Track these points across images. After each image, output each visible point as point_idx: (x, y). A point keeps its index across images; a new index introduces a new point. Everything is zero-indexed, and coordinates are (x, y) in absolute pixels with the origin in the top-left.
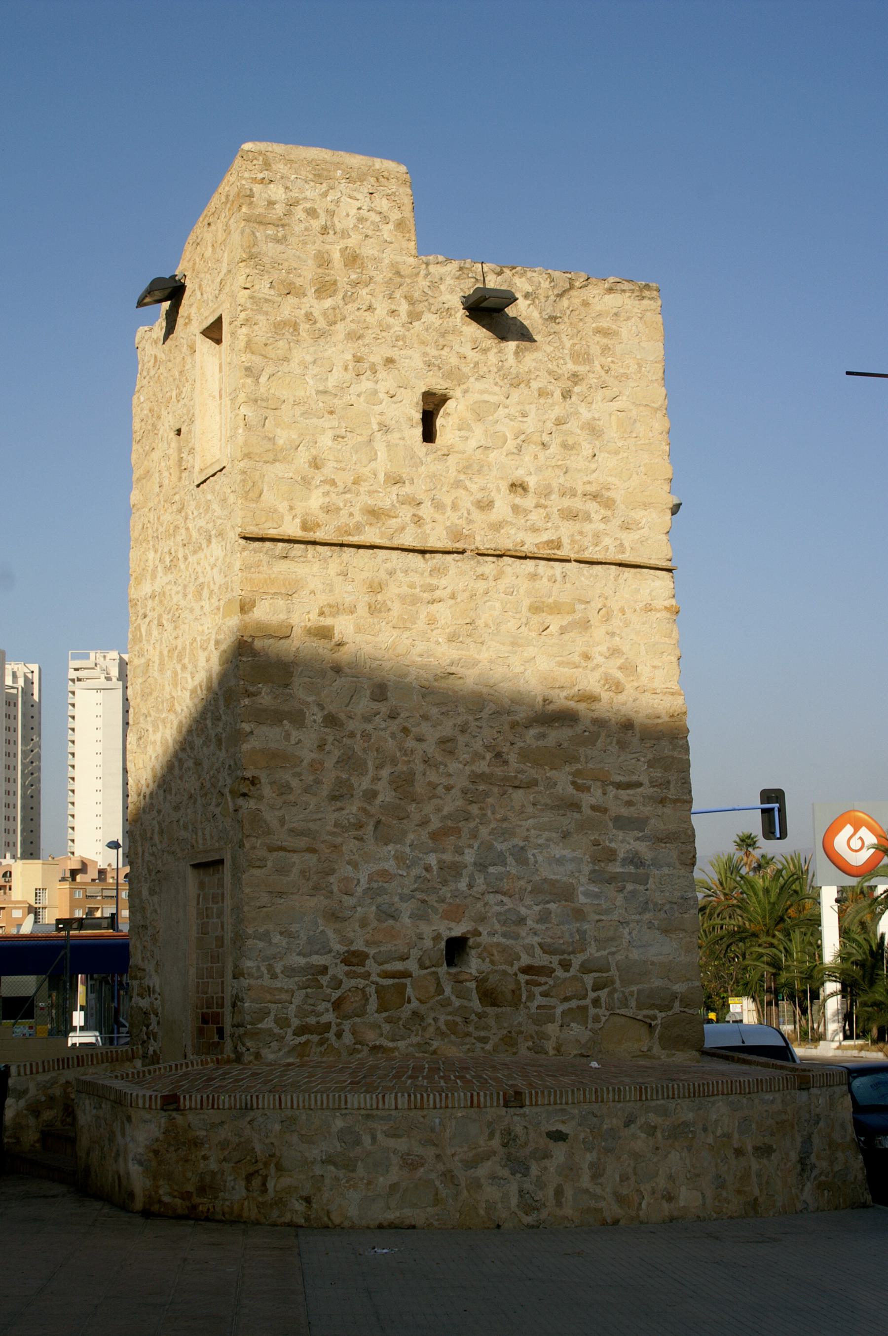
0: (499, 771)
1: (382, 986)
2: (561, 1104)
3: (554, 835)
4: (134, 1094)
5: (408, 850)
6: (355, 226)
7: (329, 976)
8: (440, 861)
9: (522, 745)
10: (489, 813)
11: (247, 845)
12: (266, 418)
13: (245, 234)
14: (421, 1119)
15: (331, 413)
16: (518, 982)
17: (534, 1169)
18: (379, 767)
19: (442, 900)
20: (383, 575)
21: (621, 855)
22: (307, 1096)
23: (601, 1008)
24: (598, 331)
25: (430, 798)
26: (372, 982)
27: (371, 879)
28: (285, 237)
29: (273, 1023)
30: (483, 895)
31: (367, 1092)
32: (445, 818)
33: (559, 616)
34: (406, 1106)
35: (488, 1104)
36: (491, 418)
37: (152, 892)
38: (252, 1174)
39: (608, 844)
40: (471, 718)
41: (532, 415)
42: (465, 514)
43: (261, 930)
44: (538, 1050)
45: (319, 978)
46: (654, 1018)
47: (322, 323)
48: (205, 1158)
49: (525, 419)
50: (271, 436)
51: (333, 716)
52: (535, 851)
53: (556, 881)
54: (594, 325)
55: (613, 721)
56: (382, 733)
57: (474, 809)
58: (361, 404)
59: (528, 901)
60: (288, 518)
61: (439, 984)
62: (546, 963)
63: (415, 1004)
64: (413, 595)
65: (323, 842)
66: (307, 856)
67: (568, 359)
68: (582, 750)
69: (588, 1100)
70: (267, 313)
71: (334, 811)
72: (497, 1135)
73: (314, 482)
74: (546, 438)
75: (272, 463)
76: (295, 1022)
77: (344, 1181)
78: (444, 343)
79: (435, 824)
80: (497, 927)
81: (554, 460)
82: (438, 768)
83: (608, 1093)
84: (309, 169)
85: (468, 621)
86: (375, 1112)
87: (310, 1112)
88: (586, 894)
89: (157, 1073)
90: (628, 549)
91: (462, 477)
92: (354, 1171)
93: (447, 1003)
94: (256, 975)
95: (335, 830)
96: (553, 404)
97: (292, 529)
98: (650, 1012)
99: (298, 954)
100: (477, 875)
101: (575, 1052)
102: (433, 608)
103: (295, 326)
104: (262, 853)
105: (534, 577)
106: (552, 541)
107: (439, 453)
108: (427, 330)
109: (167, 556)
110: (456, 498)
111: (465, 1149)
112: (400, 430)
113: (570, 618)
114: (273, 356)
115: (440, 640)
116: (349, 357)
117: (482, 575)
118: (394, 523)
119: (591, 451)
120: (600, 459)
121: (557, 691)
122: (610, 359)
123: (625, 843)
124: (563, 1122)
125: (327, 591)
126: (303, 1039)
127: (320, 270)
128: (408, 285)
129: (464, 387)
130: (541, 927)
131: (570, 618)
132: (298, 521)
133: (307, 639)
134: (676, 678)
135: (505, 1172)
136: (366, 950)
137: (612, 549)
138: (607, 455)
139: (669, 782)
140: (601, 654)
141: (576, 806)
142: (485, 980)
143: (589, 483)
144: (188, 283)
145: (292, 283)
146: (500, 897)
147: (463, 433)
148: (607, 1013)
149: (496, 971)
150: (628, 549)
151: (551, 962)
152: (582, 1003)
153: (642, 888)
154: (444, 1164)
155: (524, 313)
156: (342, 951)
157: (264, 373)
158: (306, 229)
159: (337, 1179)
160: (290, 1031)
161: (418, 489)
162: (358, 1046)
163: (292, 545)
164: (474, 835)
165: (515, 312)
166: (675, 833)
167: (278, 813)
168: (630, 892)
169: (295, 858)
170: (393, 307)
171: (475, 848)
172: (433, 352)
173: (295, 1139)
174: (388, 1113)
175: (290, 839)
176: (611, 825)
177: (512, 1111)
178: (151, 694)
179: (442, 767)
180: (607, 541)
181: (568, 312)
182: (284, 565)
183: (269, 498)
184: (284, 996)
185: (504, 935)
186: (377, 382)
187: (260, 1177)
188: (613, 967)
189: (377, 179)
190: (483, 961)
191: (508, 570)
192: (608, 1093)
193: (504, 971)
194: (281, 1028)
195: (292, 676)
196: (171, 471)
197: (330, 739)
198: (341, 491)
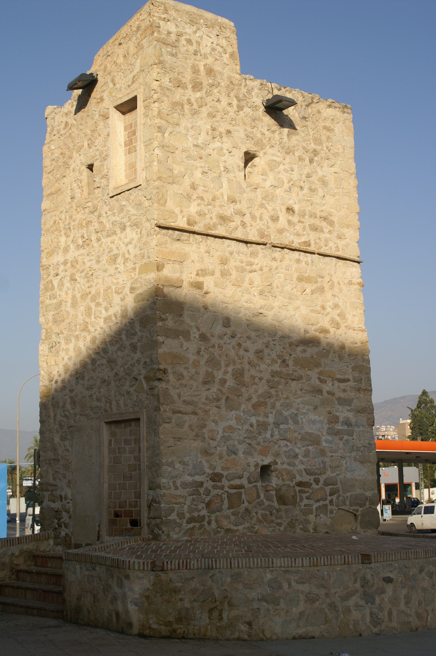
0: (284, 370)
1: (230, 493)
2: (389, 561)
3: (311, 407)
4: (132, 562)
5: (242, 414)
6: (210, 53)
7: (204, 488)
8: (258, 421)
9: (295, 356)
10: (280, 394)
11: (162, 410)
12: (168, 158)
13: (157, 48)
14: (317, 572)
15: (201, 158)
16: (295, 491)
17: (378, 601)
18: (227, 365)
19: (259, 444)
20: (227, 254)
21: (341, 419)
22: (248, 560)
23: (333, 505)
24: (325, 128)
25: (252, 385)
26: (225, 491)
27: (224, 431)
28: (176, 53)
29: (176, 516)
30: (278, 441)
31: (283, 557)
32: (259, 396)
33: (311, 284)
34: (308, 564)
35: (353, 562)
36: (277, 170)
37: (63, 439)
38: (212, 609)
39: (335, 413)
40: (271, 339)
41: (296, 170)
42: (266, 223)
43: (170, 460)
44: (305, 530)
45: (199, 489)
46: (357, 511)
47: (195, 106)
48: (181, 600)
49: (292, 172)
50: (171, 168)
51: (204, 335)
52: (302, 416)
53: (312, 433)
54: (323, 124)
55: (336, 345)
56: (228, 346)
57: (273, 391)
58: (215, 154)
59: (299, 445)
60: (180, 217)
61: (258, 493)
62: (308, 480)
63: (246, 504)
64: (242, 267)
65: (200, 408)
66: (193, 416)
67: (311, 141)
68: (322, 360)
69: (402, 558)
70: (168, 96)
71: (206, 390)
72: (359, 580)
73: (193, 198)
74: (302, 184)
75: (172, 184)
76: (187, 515)
77: (272, 611)
78: (255, 125)
79: (255, 400)
80: (285, 459)
81: (306, 197)
82: (256, 367)
83: (412, 554)
84: (187, 16)
85: (269, 284)
86: (290, 569)
87: (250, 570)
88: (326, 441)
89: (112, 548)
90: (341, 249)
91: (264, 202)
92: (278, 605)
93: (261, 504)
94: (167, 487)
95: (206, 402)
96: (305, 166)
97: (182, 223)
98: (356, 508)
99: (189, 475)
100: (275, 429)
101: (325, 531)
102: (252, 275)
103: (182, 105)
104: (169, 414)
105: (298, 261)
106: (306, 242)
107: (253, 187)
108: (246, 116)
109: (80, 239)
110: (261, 213)
111: (342, 589)
112: (234, 172)
113: (315, 286)
114: (171, 122)
115: (256, 294)
116: (209, 127)
117: (275, 258)
118: (233, 225)
119: (322, 194)
120: (327, 199)
121: (310, 326)
122: (330, 144)
123: (343, 413)
124: (391, 572)
125: (200, 261)
126: (191, 525)
127: (194, 75)
128: (236, 90)
129: (264, 151)
130: (305, 460)
131: (315, 286)
132: (185, 219)
133: (190, 289)
134: (363, 322)
135: (362, 603)
136: (222, 472)
137: (333, 249)
138: (330, 197)
139: (361, 379)
140: (330, 307)
141: (320, 391)
142: (280, 490)
143: (322, 211)
144: (99, 78)
145: (180, 81)
146: (285, 442)
147: (264, 177)
148: (336, 509)
149: (285, 485)
150: (341, 249)
151: (310, 480)
152: (325, 503)
153: (351, 438)
154: (330, 599)
155: (291, 113)
156: (210, 473)
157: (167, 131)
158: (187, 51)
159: (268, 610)
160: (185, 521)
161: (243, 206)
162: (219, 529)
163: (182, 233)
164: (273, 407)
165: (287, 112)
166: (365, 408)
167: (178, 391)
168: (346, 440)
169: (186, 417)
170: (230, 102)
171: (274, 414)
172: (250, 130)
173: (240, 586)
174: (297, 569)
175: (183, 406)
176: (336, 402)
177: (365, 565)
178: (63, 321)
179: (258, 366)
180: (331, 244)
181: (311, 115)
182: (178, 245)
183: (170, 204)
184: (182, 500)
185: (288, 464)
186: (222, 143)
187: (218, 611)
188: (339, 483)
189: (220, 28)
190: (279, 478)
191: (286, 256)
192: (412, 554)
193: (289, 484)
194: (180, 519)
195: (183, 310)
196: (83, 189)
197: (203, 348)
198: (206, 204)
